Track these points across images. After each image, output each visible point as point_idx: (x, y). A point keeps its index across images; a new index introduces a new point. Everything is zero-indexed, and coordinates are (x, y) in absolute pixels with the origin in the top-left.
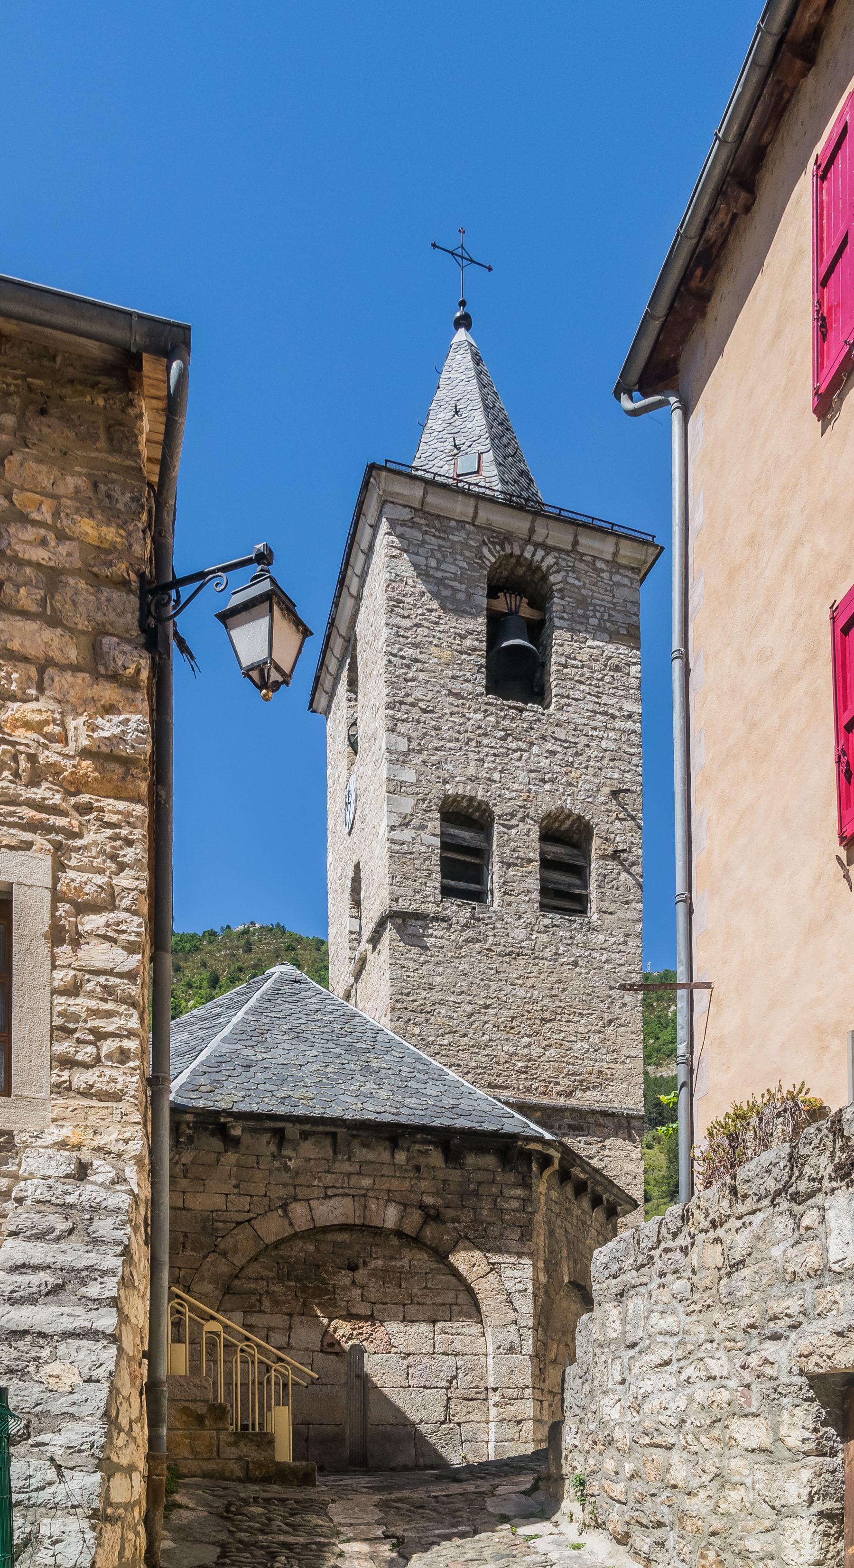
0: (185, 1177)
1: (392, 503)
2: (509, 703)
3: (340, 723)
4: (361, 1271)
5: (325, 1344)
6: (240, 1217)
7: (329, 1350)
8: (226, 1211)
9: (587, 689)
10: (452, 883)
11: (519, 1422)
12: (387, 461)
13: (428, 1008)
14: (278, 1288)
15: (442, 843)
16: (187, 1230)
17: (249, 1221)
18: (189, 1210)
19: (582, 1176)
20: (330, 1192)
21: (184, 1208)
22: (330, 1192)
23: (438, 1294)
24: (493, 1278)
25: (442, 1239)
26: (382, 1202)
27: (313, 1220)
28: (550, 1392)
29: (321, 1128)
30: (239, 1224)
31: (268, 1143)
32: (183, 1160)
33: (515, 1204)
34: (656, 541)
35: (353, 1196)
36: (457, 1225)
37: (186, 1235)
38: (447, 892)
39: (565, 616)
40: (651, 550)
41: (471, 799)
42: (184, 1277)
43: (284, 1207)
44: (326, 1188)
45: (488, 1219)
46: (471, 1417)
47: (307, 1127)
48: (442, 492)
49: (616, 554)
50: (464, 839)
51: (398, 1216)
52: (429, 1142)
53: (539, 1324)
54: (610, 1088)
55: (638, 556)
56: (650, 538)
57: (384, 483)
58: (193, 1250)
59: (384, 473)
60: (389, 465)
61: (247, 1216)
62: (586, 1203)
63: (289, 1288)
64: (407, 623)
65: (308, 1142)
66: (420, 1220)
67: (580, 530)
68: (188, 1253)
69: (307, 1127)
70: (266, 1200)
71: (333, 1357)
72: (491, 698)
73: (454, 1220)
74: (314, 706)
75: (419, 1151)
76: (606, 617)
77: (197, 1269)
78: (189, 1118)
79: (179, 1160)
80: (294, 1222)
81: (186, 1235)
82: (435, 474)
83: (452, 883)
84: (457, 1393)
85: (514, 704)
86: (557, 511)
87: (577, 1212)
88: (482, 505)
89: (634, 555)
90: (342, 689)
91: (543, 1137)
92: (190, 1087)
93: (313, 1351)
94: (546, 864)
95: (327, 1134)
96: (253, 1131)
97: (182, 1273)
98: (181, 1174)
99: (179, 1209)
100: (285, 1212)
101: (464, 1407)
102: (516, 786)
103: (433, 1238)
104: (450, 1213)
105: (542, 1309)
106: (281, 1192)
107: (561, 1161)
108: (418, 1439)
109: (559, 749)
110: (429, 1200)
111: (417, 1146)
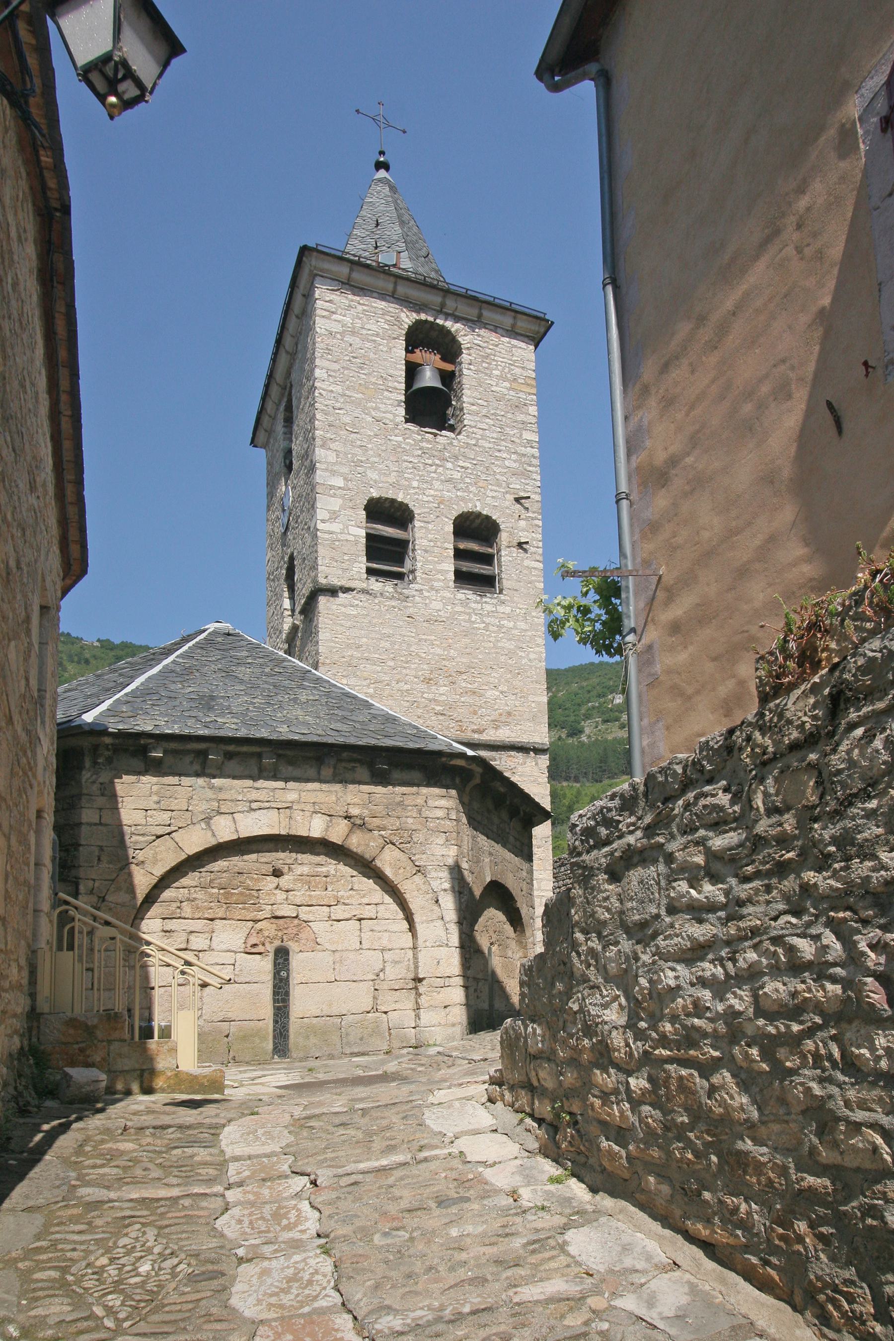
0: (103, 795)
1: (322, 276)
2: (427, 430)
3: (277, 451)
4: (286, 877)
5: (248, 946)
6: (160, 831)
7: (253, 950)
8: (146, 825)
9: (492, 422)
10: (375, 566)
11: (360, 920)
12: (317, 245)
13: (354, 663)
14: (200, 895)
15: (367, 534)
16: (104, 844)
17: (169, 834)
18: (106, 825)
19: (502, 790)
20: (255, 805)
21: (101, 824)
22: (255, 805)
23: (364, 896)
24: (418, 879)
25: (368, 845)
26: (308, 814)
27: (237, 831)
28: (475, 979)
29: (245, 749)
30: (158, 837)
31: (192, 763)
32: (101, 780)
33: (440, 813)
34: (547, 317)
35: (278, 809)
36: (383, 833)
37: (101, 848)
38: (370, 572)
39: (472, 367)
40: (543, 323)
41: (393, 501)
42: (98, 888)
43: (208, 820)
44: (251, 802)
45: (414, 827)
46: (396, 1006)
47: (231, 748)
48: (366, 270)
49: (513, 326)
50: (387, 532)
51: (324, 826)
52: (355, 761)
53: (465, 918)
54: (519, 727)
55: (533, 328)
56: (542, 315)
57: (313, 262)
58: (110, 862)
59: (315, 254)
60: (320, 248)
61: (168, 830)
62: (505, 815)
63: (211, 895)
64: (336, 366)
65: (232, 761)
66: (346, 830)
67: (484, 305)
68: (104, 865)
69: (231, 748)
70: (189, 814)
71: (258, 956)
72: (410, 426)
73: (380, 829)
74: (255, 442)
75: (345, 768)
76: (507, 370)
77: (113, 880)
78: (108, 740)
79: (97, 779)
80: (216, 833)
81: (101, 848)
82: (359, 257)
83: (375, 566)
84: (385, 986)
85: (430, 430)
86: (464, 291)
87: (496, 820)
88: (399, 281)
89: (529, 327)
90: (280, 428)
91: (466, 754)
92: (111, 713)
93: (236, 952)
94: (459, 554)
95: (252, 754)
96: (175, 752)
97: (97, 884)
98: (98, 792)
99: (96, 824)
100: (208, 825)
101: (391, 996)
102: (432, 492)
103: (359, 845)
104: (376, 822)
105: (467, 906)
106: (204, 806)
107: (482, 775)
108: (472, 512)
109: (469, 465)
110: (355, 811)
111: (344, 764)
